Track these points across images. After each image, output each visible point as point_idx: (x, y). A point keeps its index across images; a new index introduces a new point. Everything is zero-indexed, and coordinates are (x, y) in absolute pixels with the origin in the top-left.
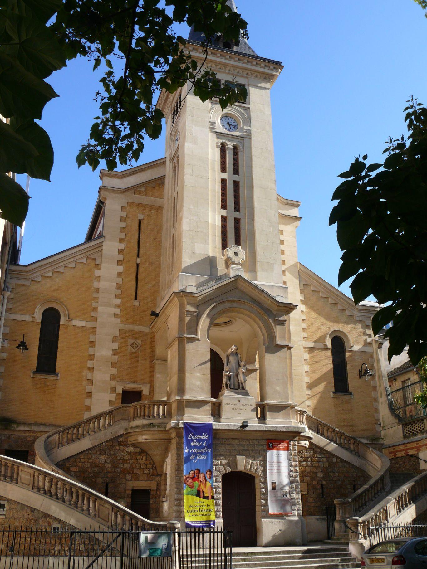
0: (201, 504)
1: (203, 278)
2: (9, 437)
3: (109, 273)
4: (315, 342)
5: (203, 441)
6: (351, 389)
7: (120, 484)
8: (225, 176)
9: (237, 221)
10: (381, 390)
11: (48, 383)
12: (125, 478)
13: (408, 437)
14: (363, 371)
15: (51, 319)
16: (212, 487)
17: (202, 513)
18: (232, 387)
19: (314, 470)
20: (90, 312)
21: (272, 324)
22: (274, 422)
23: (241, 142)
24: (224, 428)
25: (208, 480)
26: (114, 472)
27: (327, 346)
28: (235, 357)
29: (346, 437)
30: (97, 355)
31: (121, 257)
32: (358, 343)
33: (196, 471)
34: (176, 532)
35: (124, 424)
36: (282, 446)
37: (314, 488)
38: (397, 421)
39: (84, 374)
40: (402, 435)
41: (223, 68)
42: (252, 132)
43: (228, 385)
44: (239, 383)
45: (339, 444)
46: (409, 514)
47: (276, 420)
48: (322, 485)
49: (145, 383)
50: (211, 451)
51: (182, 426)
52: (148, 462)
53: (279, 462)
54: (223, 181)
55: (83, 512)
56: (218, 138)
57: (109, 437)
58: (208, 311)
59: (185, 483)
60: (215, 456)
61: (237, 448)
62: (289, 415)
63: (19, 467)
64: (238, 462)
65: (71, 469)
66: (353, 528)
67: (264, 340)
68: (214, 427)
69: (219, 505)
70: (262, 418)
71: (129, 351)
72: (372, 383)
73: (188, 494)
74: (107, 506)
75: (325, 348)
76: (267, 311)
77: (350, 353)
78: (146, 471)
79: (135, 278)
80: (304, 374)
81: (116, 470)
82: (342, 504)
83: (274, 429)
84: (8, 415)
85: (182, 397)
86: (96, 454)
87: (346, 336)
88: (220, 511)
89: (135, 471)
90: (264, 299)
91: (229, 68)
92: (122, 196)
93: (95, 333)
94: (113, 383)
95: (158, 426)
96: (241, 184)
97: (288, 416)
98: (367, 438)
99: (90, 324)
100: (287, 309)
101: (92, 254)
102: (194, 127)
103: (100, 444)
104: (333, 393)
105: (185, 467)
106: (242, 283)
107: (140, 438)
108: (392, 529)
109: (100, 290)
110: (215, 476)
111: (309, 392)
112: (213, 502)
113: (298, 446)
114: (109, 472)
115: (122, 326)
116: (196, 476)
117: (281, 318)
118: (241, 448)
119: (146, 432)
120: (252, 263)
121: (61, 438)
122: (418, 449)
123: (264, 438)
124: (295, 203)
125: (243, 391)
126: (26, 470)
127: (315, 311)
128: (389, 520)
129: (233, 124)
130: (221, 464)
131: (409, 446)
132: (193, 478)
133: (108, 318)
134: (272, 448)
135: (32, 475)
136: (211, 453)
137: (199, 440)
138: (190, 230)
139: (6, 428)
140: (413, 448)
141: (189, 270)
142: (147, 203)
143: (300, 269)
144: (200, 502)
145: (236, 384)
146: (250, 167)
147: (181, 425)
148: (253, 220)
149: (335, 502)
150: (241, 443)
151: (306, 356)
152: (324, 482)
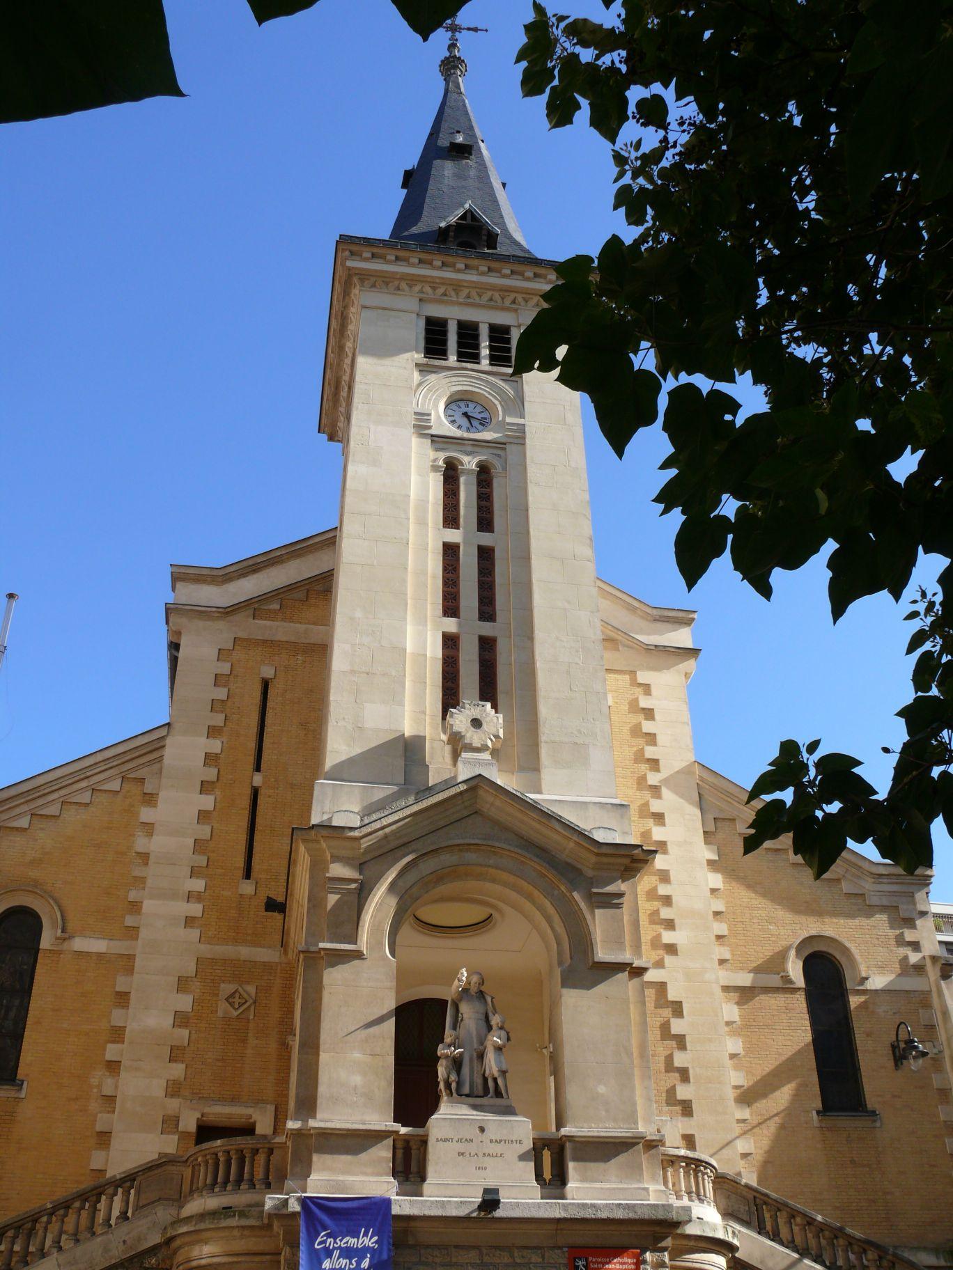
1: (381, 792)
3: (178, 815)
4: (757, 970)
6: (872, 1101)
8: (454, 536)
9: (487, 646)
14: (902, 1045)
18: (466, 1090)
20: (120, 914)
21: (582, 905)
23: (499, 456)
24: (427, 1212)
27: (791, 982)
28: (478, 1006)
29: (851, 1242)
30: (132, 1027)
31: (211, 774)
32: (882, 968)
35: (163, 1214)
39: (94, 1081)
41: (453, 293)
42: (527, 429)
43: (454, 1085)
44: (485, 1080)
47: (598, 1185)
49: (264, 1102)
51: (298, 1208)
54: (450, 551)
56: (437, 450)
57: (117, 1253)
62: (641, 1175)
67: (560, 953)
68: (395, 1210)
70: (554, 1182)
71: (220, 1014)
72: (936, 1081)
75: (786, 987)
76: (569, 872)
77: (862, 999)
79: (244, 823)
80: (728, 1063)
83: (589, 1214)
85: (305, 1121)
87: (846, 951)
90: (555, 837)
91: (466, 291)
92: (221, 624)
93: (130, 971)
94: (173, 1104)
95: (242, 1214)
96: (498, 554)
97: (635, 1171)
98: (936, 1251)
99: (119, 947)
100: (627, 861)
102: (372, 427)
104: (818, 1112)
106: (490, 799)
107: (196, 1252)
111: (745, 1113)
115: (206, 950)
117: (610, 889)
119: (208, 1234)
120: (525, 746)
124: (681, 615)
125: (498, 1101)
129: (479, 416)
133: (168, 931)
137: (348, 1253)
138: (353, 672)
141: (344, 772)
142: (284, 639)
143: (702, 779)
145: (479, 1081)
146: (524, 510)
147: (294, 1206)
148: (531, 638)
150: (486, 1259)
151: (731, 1011)
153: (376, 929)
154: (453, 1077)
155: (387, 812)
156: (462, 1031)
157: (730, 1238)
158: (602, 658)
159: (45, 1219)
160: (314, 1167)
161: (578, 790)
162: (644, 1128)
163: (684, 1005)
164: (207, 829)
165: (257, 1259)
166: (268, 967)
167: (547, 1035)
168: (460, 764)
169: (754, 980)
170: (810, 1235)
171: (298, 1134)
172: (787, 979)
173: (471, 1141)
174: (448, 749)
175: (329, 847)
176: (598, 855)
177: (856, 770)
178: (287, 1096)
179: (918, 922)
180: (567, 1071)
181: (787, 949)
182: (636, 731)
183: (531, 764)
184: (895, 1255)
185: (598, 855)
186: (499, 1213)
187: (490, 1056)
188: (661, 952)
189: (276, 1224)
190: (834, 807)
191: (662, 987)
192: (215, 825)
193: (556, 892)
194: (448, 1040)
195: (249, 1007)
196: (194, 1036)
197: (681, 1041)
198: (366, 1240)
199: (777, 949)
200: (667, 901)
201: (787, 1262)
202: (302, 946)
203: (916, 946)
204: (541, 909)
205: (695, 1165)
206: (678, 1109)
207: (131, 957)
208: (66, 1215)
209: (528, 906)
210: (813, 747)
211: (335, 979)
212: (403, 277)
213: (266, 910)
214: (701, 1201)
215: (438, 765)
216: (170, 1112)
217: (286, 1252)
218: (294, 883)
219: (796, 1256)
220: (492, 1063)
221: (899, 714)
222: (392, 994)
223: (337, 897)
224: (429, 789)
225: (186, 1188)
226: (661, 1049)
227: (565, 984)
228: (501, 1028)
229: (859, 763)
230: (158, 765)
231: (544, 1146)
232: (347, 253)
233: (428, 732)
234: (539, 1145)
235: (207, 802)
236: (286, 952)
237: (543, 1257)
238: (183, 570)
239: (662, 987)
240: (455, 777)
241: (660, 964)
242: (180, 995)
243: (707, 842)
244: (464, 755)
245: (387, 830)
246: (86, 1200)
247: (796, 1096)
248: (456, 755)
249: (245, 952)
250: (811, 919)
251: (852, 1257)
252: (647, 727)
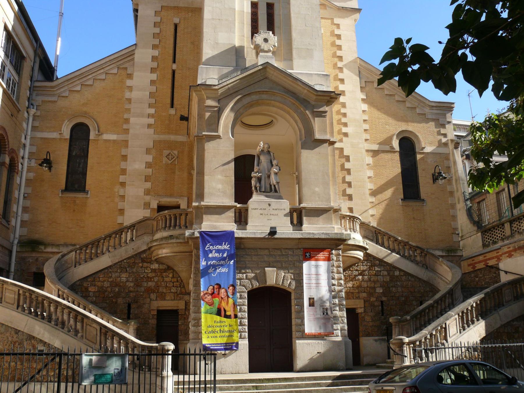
0: (222, 324)
1: (226, 70)
2: (37, 259)
3: (142, 82)
4: (380, 144)
5: (223, 251)
6: (423, 195)
7: (144, 304)
10: (458, 195)
11: (77, 202)
12: (149, 297)
13: (488, 246)
15: (80, 134)
16: (235, 305)
17: (223, 334)
18: (263, 190)
19: (372, 285)
20: (121, 124)
21: (310, 116)
22: (312, 228)
24: (248, 236)
25: (231, 296)
26: (137, 291)
27: (394, 148)
28: (267, 156)
29: (411, 247)
30: (129, 168)
31: (155, 65)
32: (431, 144)
33: (216, 286)
34: (170, 354)
35: (147, 239)
36: (321, 255)
37: (372, 305)
38: (476, 228)
39: (116, 190)
40: (481, 244)
43: (258, 188)
44: (271, 186)
45: (403, 256)
46: (477, 332)
47: (315, 226)
48: (382, 302)
49: (183, 196)
50: (234, 263)
51: (198, 235)
52: (175, 280)
53: (317, 274)
55: (69, 334)
57: (131, 253)
58: (231, 104)
59: (203, 300)
60: (239, 268)
61: (266, 259)
63: (3, 285)
64: (267, 275)
65: (90, 289)
66: (397, 350)
68: (236, 235)
69: (245, 325)
70: (298, 224)
71: (164, 162)
72: (449, 188)
73: (206, 313)
74: (94, 325)
75: (392, 151)
76: (305, 102)
77: (422, 156)
78: (173, 290)
79: (170, 85)
80: (367, 180)
81: (139, 289)
82: (399, 322)
83: (311, 236)
84: (36, 237)
86: (117, 272)
87: (416, 136)
88: (245, 332)
89: (161, 290)
90: (300, 88)
93: (127, 146)
94: (148, 198)
95: (177, 238)
97: (330, 221)
98: (442, 250)
99: (122, 137)
100: (328, 98)
101: (123, 64)
103: (121, 261)
104: (402, 200)
105: (202, 281)
106: (272, 72)
108: (450, 350)
109: (132, 101)
110: (239, 292)
111: (373, 199)
112: (236, 322)
113: (343, 256)
114: (131, 292)
115: (157, 137)
116: (215, 292)
117: (321, 109)
118: (271, 259)
120: (286, 50)
121: (78, 257)
122: (499, 259)
123: (300, 246)
125: (276, 194)
126: (11, 288)
127: (379, 110)
128: (449, 340)
130: (247, 278)
131: (489, 256)
132: (212, 294)
133: (141, 129)
134: (309, 259)
135: (17, 293)
136: (234, 266)
137: (218, 251)
138: (213, 19)
139: (33, 250)
140: (493, 258)
141: (210, 62)
142: (183, 6)
144: (221, 322)
145: (268, 186)
147: (197, 235)
149: (391, 320)
150: (271, 253)
151: (369, 160)
152: (384, 299)
153: (225, 127)
154: (258, 185)
155: (229, 78)
156: (261, 167)
157: (365, 246)
158: (319, 12)
159: (102, 241)
160: (204, 220)
161: (308, 68)
162: (333, 204)
163: (350, 157)
164: (155, 88)
165: (183, 254)
166: (182, 143)
167: (295, 167)
168: (259, 58)
169: (379, 148)
170: (396, 245)
171: (197, 207)
172: (392, 148)
174: (254, 51)
175: (205, 93)
176: (317, 95)
177: (427, 51)
178: (192, 194)
179: (447, 126)
180: (303, 182)
181: (393, 135)
182: (333, 44)
183: (289, 57)
184: (427, 252)
185: (317, 95)
186: (276, 236)
187: (273, 177)
188: (342, 136)
189: (190, 242)
190: (416, 67)
191: (341, 150)
194: (255, 170)
195: (175, 160)
197: (349, 171)
198: (225, 246)
199: (389, 136)
200: (345, 115)
201: (386, 254)
202: (196, 134)
203: (445, 135)
204: (293, 117)
205: (353, 219)
206: (347, 198)
207: (127, 141)
208: (110, 240)
209: (288, 117)
210: (408, 41)
211: (210, 147)
213: (181, 120)
214: (354, 232)
215: (250, 58)
216: (147, 201)
217: (195, 251)
218: (191, 105)
219: (390, 252)
220: (273, 180)
221: (447, 27)
222: (233, 152)
223: (210, 113)
224: (246, 68)
225: (155, 229)
226: (340, 175)
227: (302, 148)
228: (277, 165)
229: (428, 48)
230: (132, 62)
231: (294, 211)
233: (245, 45)
234: (292, 211)
235: (154, 77)
236: (189, 137)
237: (293, 252)
239: (341, 150)
240: (257, 63)
241: (341, 141)
243: (361, 91)
244: (261, 54)
245: (229, 86)
246: (117, 234)
247: (394, 193)
248: (257, 54)
249: (172, 137)
250: (403, 123)
251: (411, 252)
252: (338, 42)
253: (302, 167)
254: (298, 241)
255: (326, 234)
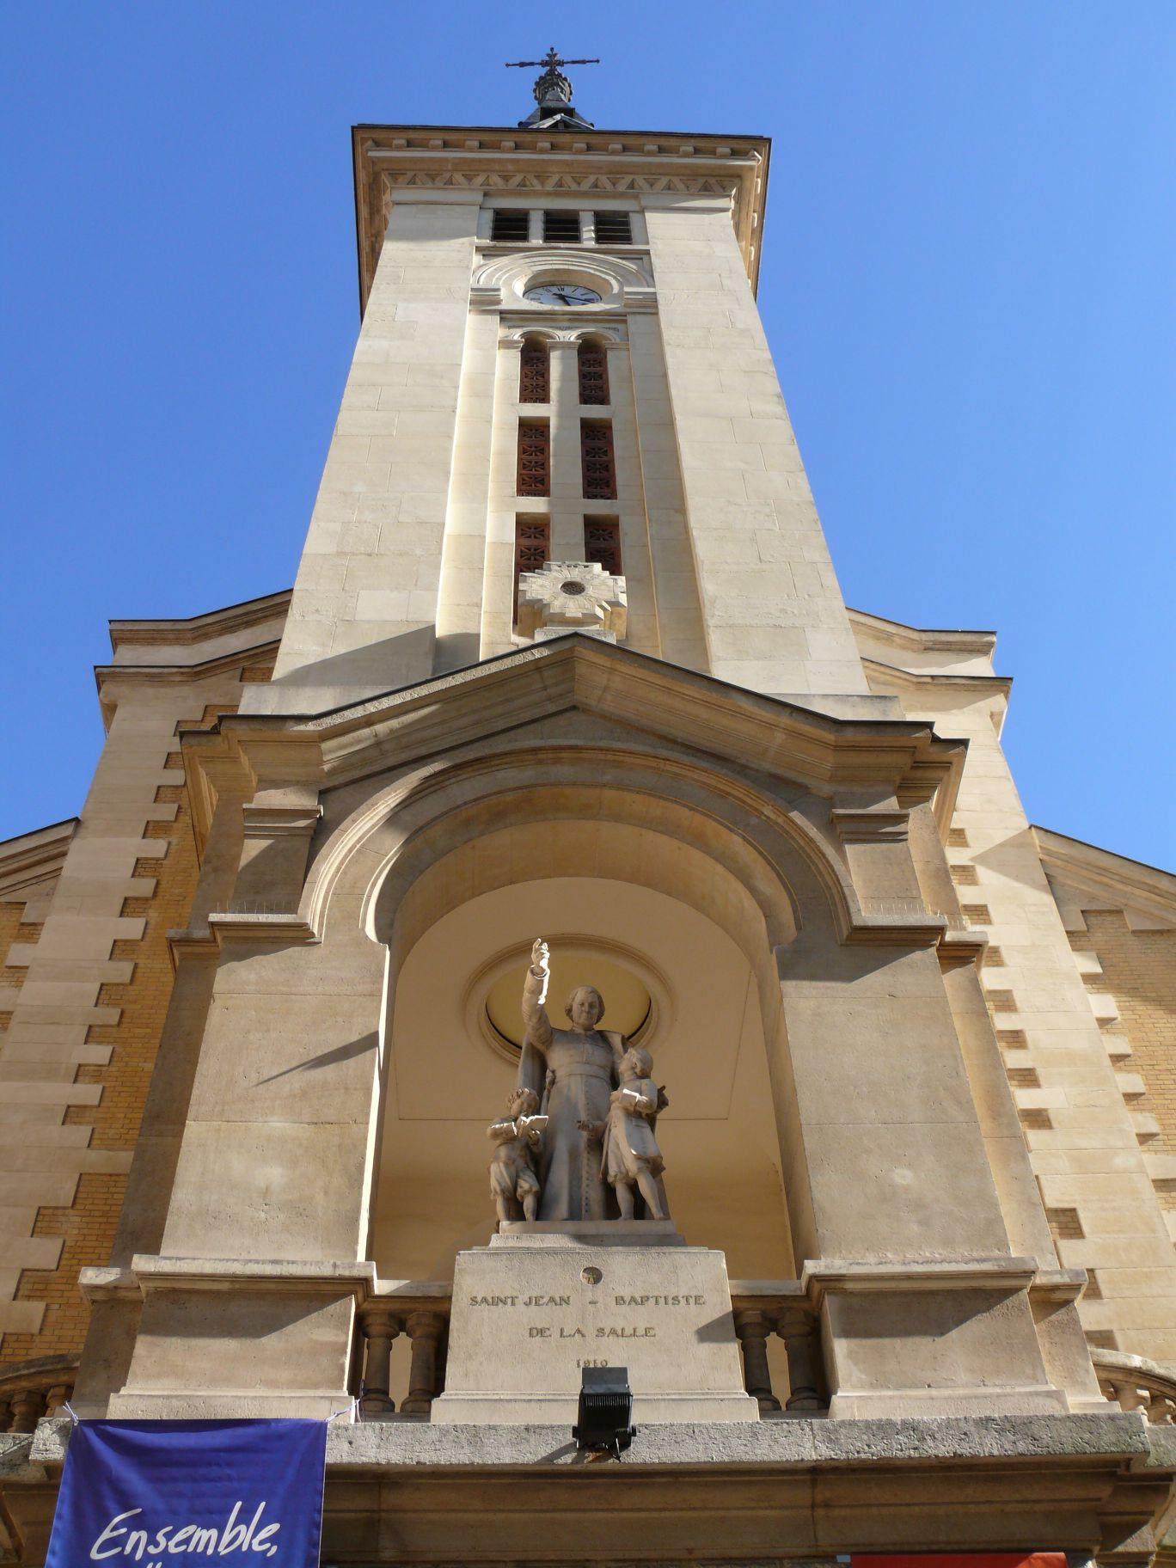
31: (145, 886)
41: (535, 182)
43: (529, 1203)
44: (609, 1191)
62: (1036, 1363)
68: (337, 1453)
70: (815, 1390)
83: (900, 1448)
92: (186, 690)
97: (1024, 1356)
100: (904, 760)
106: (602, 679)
115: (98, 1160)
125: (641, 1226)
138: (341, 554)
154: (527, 1183)
160: (135, 1367)
173: (565, 1301)
176: (838, 748)
185: (838, 748)
192: (141, 962)
193: (754, 821)
196: (52, 1318)
198: (245, 1533)
211: (239, 985)
212: (459, 165)
223: (265, 843)
227: (787, 973)
230: (51, 883)
232: (370, 143)
234: (752, 1316)
238: (129, 626)
242: (36, 1240)
243: (1076, 948)
253: (796, 1062)
254: (802, 1495)
255: (1011, 1425)
